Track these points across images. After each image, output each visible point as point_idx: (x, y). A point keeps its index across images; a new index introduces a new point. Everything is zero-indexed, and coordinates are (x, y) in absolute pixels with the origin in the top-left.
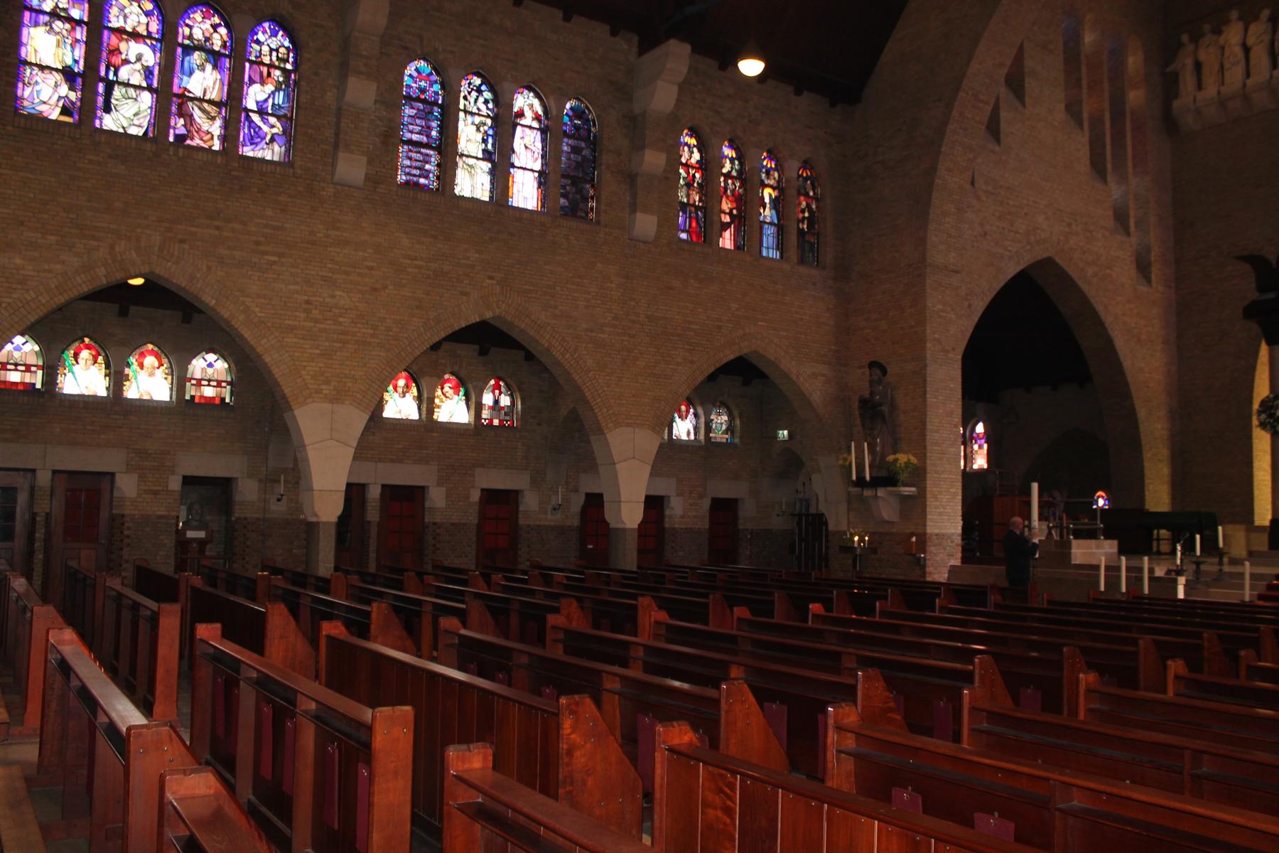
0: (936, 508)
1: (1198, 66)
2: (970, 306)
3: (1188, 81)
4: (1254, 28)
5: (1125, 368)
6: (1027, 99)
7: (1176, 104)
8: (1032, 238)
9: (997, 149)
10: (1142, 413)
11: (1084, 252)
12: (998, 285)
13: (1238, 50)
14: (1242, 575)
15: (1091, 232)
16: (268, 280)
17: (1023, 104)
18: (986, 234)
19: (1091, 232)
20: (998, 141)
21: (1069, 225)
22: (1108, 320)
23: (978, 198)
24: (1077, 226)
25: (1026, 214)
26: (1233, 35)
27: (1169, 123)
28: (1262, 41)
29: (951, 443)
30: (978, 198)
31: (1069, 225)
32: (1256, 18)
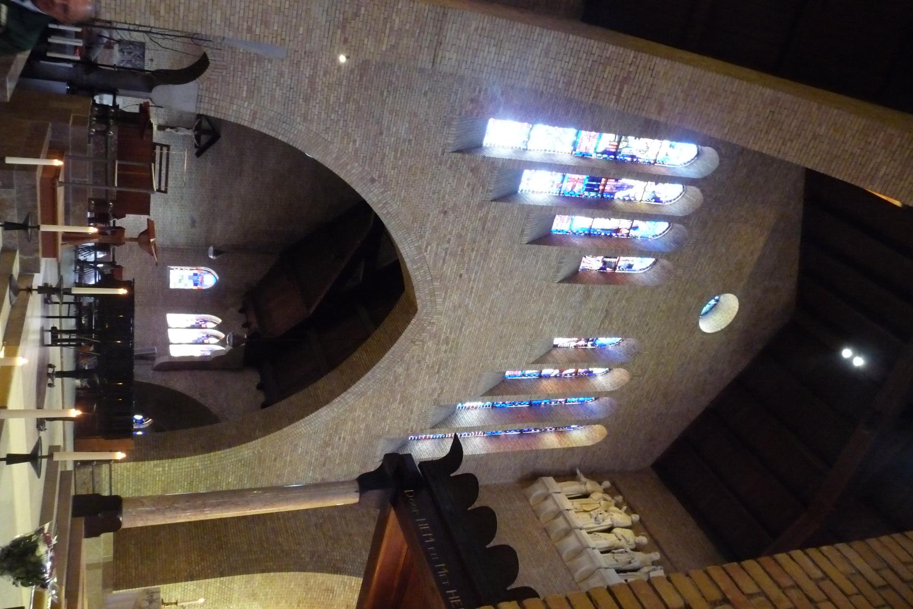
0: (117, 490)
1: (586, 496)
2: (373, 180)
3: (572, 487)
4: (629, 533)
5: (297, 423)
6: (566, 285)
7: (551, 480)
8: (437, 284)
9: (526, 239)
10: (246, 451)
11: (419, 362)
12: (391, 226)
13: (607, 523)
14: (54, 222)
15: (438, 372)
16: (296, 4)
17: (562, 281)
18: (445, 213)
19: (438, 372)
20: (530, 243)
21: (447, 342)
22: (348, 397)
23: (481, 206)
24: (445, 352)
25: (461, 276)
26: (620, 517)
27: (533, 477)
28: (620, 540)
29: (228, 15)
30: (481, 206)
31: (447, 342)
32: (637, 534)
